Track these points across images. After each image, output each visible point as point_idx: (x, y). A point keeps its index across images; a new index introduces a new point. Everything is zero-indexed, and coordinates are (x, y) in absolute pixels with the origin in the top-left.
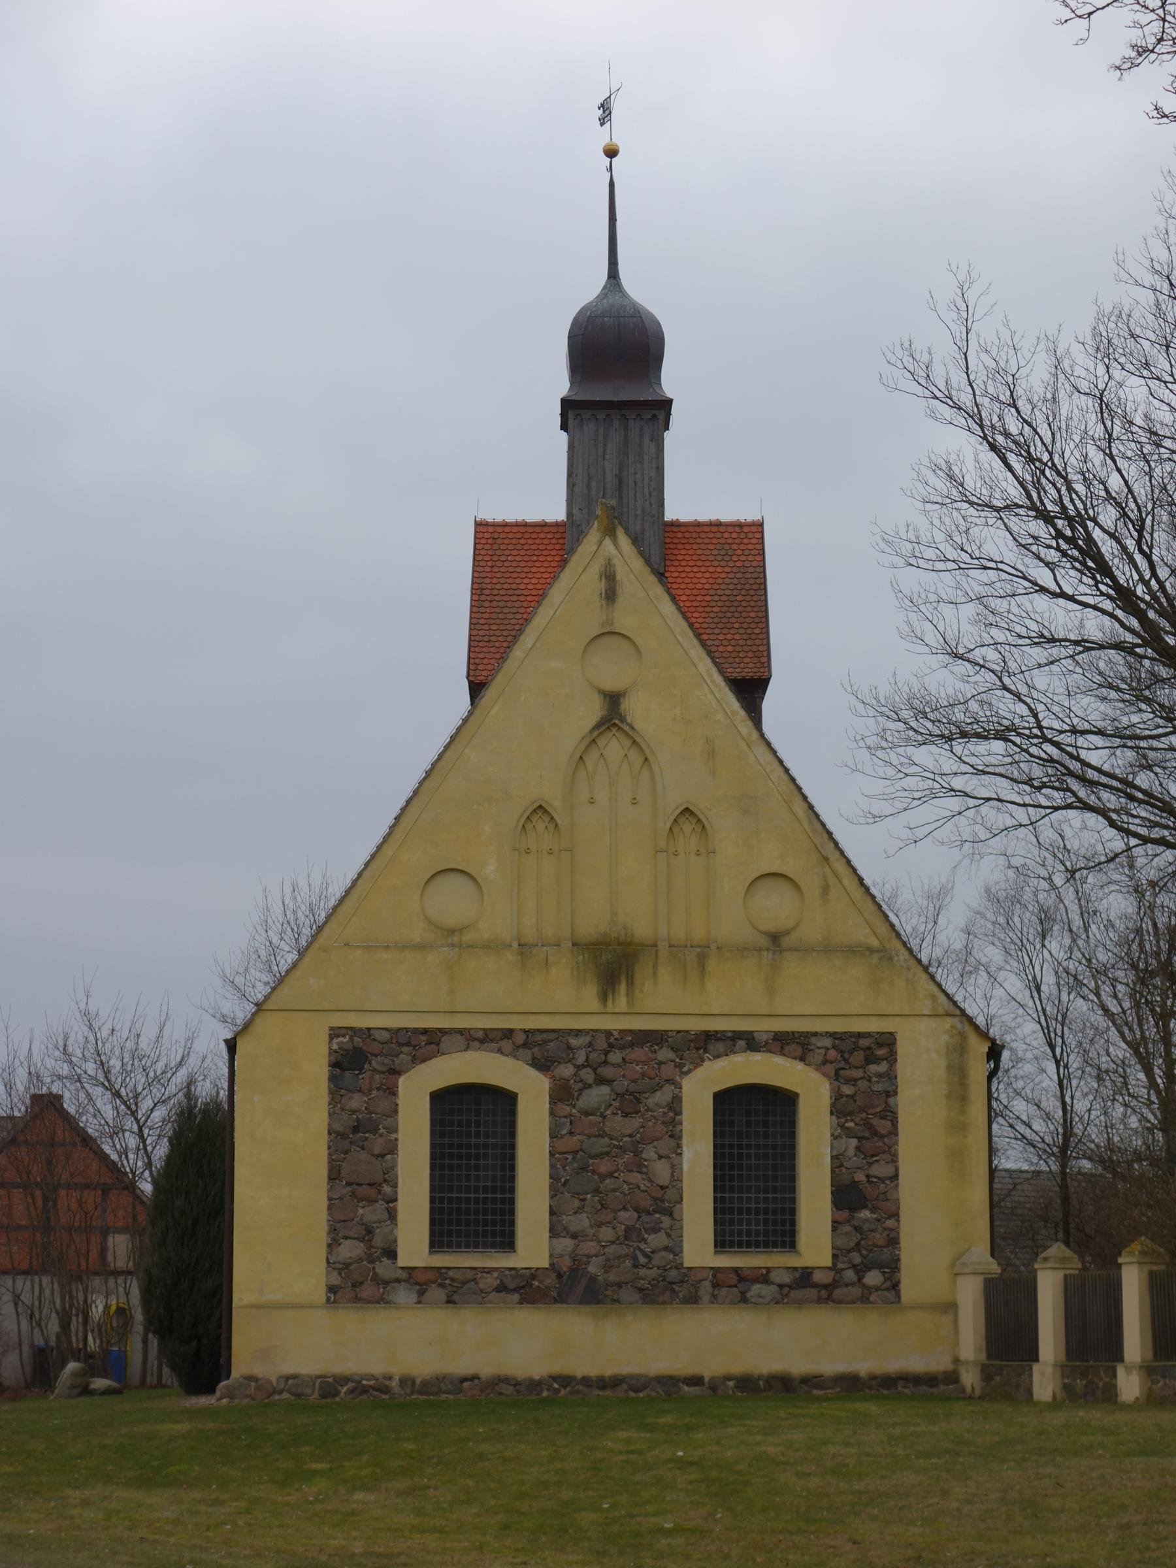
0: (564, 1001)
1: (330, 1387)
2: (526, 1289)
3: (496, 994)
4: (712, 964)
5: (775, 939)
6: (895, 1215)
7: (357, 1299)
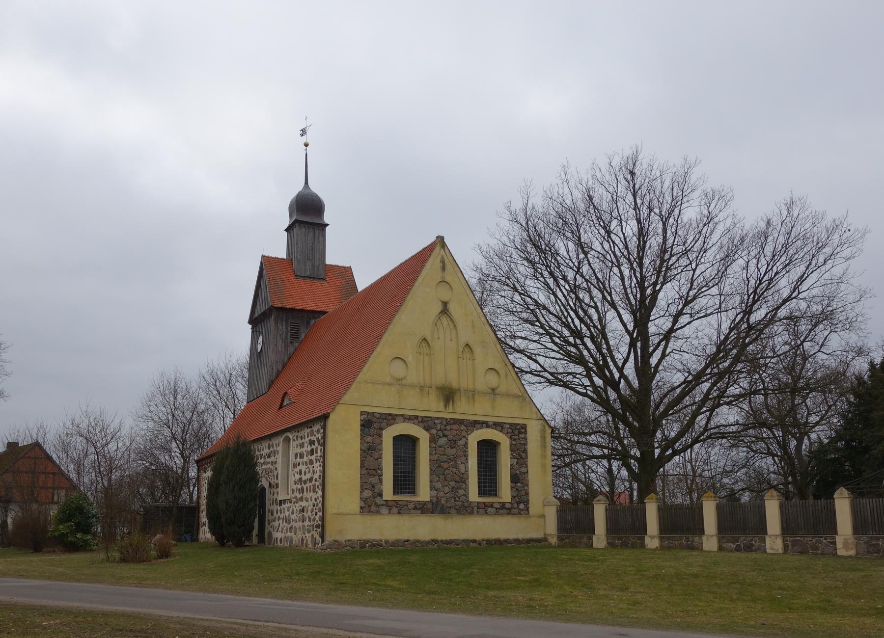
0: (433, 407)
1: (363, 544)
2: (423, 509)
3: (414, 404)
4: (476, 397)
5: (493, 390)
6: (527, 485)
7: (370, 512)
